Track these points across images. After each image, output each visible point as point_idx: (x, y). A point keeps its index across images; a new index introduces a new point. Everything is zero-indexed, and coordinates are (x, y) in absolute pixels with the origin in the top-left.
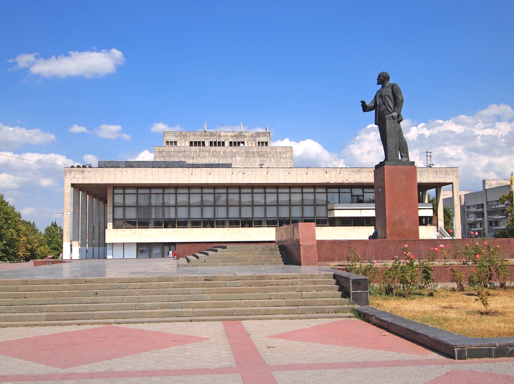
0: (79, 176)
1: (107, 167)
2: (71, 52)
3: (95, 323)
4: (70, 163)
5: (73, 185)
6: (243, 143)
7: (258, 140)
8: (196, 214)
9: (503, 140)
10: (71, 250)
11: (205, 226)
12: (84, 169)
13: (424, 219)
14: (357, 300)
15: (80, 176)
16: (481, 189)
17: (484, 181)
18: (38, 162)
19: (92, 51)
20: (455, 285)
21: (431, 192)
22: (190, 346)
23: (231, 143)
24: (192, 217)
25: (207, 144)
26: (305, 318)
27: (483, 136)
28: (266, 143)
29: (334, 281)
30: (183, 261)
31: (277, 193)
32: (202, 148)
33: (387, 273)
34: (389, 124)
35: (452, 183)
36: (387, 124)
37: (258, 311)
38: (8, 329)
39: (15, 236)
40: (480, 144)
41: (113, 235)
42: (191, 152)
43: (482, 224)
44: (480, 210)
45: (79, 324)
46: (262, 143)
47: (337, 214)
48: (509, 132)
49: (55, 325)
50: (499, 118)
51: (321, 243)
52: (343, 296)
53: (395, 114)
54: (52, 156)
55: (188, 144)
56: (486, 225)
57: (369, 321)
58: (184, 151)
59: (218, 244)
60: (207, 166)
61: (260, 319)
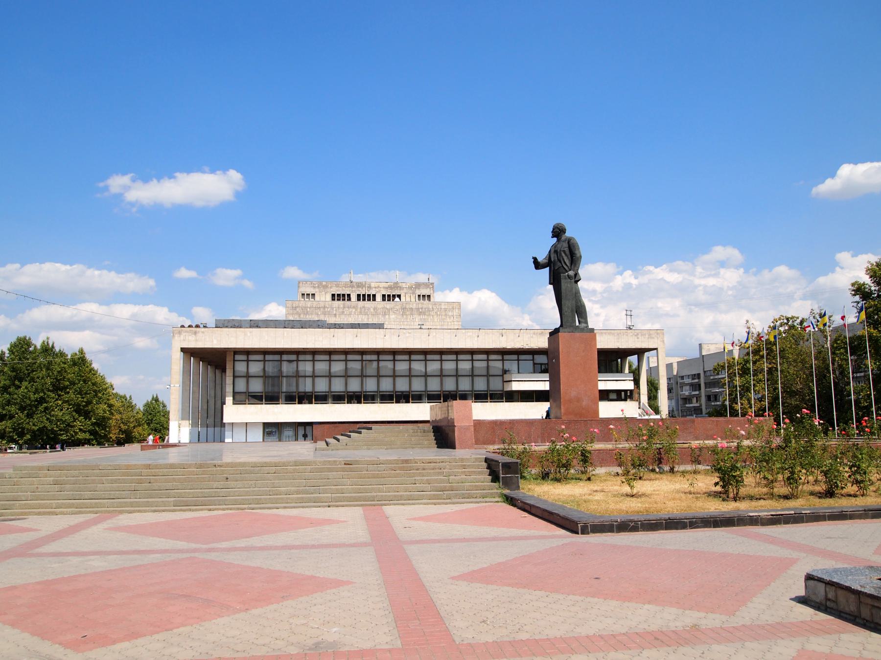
0: (190, 338)
1: (227, 327)
2: (177, 174)
3: (228, 509)
4: (178, 320)
5: (183, 350)
6: (399, 296)
7: (418, 292)
8: (338, 386)
9: (730, 292)
10: (180, 431)
11: (349, 402)
12: (198, 329)
13: (623, 393)
14: (507, 484)
15: (192, 338)
16: (698, 356)
17: (700, 345)
18: (134, 316)
19: (204, 172)
20: (619, 470)
21: (634, 359)
22: (327, 527)
23: (384, 296)
24: (333, 390)
25: (354, 297)
26: (450, 503)
27: (705, 286)
28: (429, 296)
29: (485, 465)
30: (321, 444)
31: (441, 360)
32: (347, 303)
33: (541, 459)
34: (565, 285)
35: (656, 349)
36: (563, 284)
37: (401, 496)
38: (135, 514)
39: (107, 415)
40: (702, 297)
41: (232, 412)
42: (332, 308)
43: (698, 398)
44: (696, 381)
45: (210, 510)
46: (424, 296)
47: (516, 386)
48: (738, 282)
49: (184, 511)
50: (723, 264)
51: (479, 424)
52: (493, 481)
53: (571, 273)
54: (151, 308)
55: (329, 297)
56: (703, 399)
57: (514, 505)
58: (325, 307)
59: (365, 425)
60: (353, 326)
61: (403, 504)
